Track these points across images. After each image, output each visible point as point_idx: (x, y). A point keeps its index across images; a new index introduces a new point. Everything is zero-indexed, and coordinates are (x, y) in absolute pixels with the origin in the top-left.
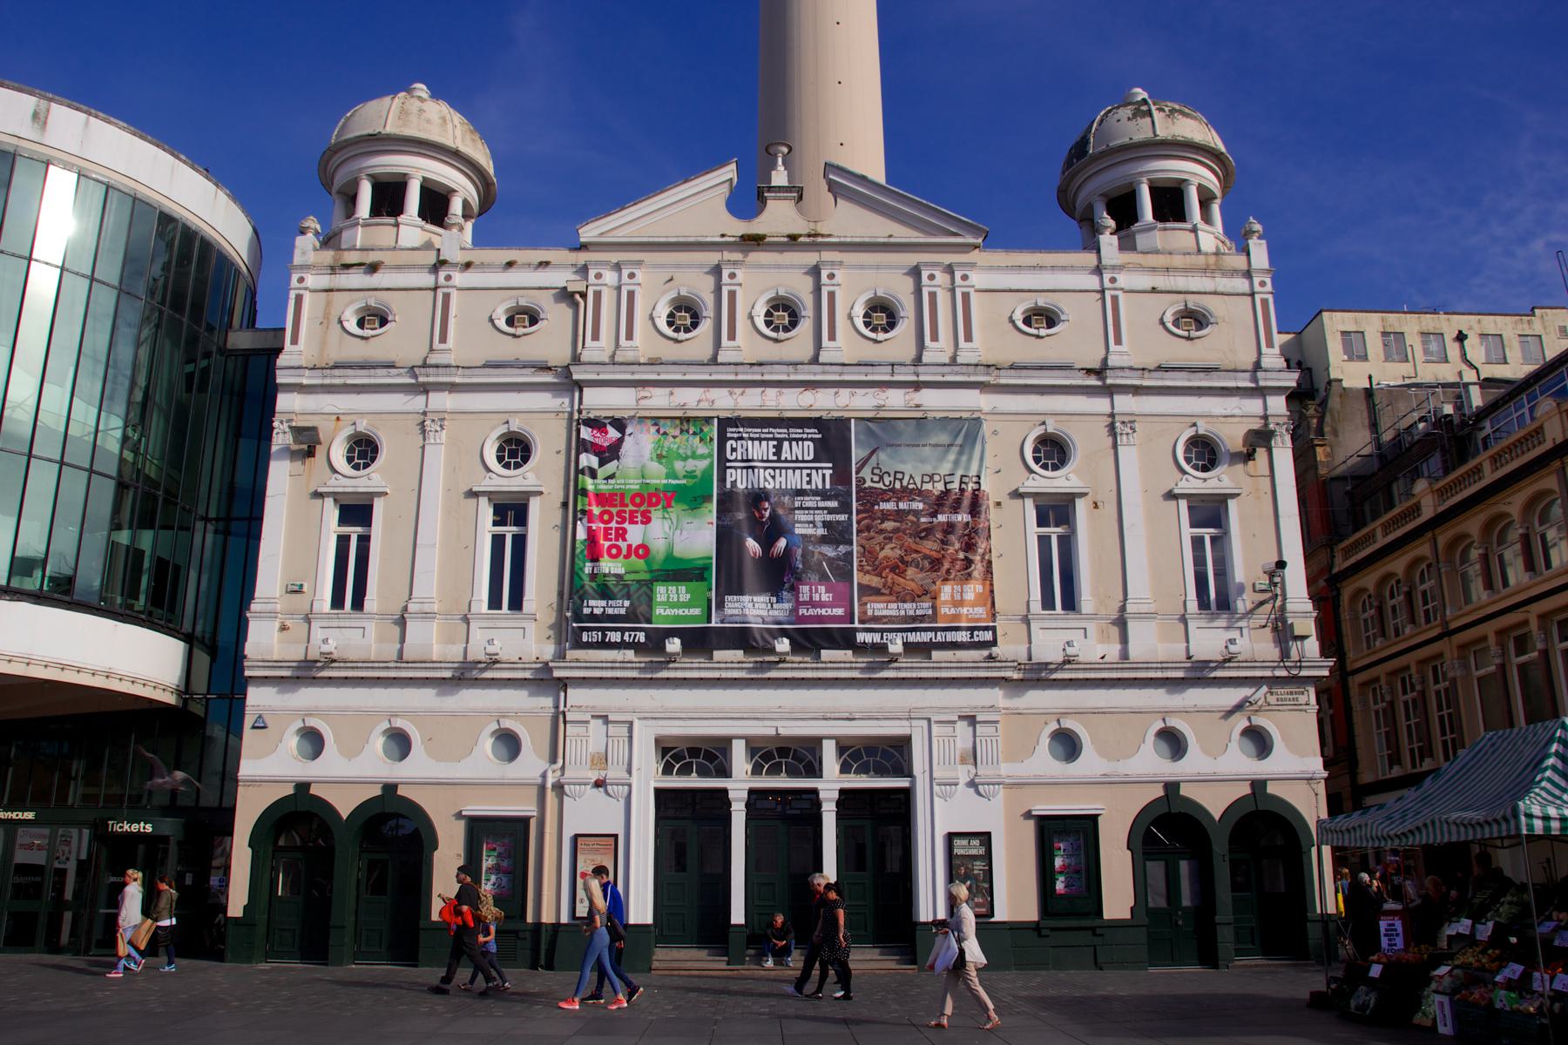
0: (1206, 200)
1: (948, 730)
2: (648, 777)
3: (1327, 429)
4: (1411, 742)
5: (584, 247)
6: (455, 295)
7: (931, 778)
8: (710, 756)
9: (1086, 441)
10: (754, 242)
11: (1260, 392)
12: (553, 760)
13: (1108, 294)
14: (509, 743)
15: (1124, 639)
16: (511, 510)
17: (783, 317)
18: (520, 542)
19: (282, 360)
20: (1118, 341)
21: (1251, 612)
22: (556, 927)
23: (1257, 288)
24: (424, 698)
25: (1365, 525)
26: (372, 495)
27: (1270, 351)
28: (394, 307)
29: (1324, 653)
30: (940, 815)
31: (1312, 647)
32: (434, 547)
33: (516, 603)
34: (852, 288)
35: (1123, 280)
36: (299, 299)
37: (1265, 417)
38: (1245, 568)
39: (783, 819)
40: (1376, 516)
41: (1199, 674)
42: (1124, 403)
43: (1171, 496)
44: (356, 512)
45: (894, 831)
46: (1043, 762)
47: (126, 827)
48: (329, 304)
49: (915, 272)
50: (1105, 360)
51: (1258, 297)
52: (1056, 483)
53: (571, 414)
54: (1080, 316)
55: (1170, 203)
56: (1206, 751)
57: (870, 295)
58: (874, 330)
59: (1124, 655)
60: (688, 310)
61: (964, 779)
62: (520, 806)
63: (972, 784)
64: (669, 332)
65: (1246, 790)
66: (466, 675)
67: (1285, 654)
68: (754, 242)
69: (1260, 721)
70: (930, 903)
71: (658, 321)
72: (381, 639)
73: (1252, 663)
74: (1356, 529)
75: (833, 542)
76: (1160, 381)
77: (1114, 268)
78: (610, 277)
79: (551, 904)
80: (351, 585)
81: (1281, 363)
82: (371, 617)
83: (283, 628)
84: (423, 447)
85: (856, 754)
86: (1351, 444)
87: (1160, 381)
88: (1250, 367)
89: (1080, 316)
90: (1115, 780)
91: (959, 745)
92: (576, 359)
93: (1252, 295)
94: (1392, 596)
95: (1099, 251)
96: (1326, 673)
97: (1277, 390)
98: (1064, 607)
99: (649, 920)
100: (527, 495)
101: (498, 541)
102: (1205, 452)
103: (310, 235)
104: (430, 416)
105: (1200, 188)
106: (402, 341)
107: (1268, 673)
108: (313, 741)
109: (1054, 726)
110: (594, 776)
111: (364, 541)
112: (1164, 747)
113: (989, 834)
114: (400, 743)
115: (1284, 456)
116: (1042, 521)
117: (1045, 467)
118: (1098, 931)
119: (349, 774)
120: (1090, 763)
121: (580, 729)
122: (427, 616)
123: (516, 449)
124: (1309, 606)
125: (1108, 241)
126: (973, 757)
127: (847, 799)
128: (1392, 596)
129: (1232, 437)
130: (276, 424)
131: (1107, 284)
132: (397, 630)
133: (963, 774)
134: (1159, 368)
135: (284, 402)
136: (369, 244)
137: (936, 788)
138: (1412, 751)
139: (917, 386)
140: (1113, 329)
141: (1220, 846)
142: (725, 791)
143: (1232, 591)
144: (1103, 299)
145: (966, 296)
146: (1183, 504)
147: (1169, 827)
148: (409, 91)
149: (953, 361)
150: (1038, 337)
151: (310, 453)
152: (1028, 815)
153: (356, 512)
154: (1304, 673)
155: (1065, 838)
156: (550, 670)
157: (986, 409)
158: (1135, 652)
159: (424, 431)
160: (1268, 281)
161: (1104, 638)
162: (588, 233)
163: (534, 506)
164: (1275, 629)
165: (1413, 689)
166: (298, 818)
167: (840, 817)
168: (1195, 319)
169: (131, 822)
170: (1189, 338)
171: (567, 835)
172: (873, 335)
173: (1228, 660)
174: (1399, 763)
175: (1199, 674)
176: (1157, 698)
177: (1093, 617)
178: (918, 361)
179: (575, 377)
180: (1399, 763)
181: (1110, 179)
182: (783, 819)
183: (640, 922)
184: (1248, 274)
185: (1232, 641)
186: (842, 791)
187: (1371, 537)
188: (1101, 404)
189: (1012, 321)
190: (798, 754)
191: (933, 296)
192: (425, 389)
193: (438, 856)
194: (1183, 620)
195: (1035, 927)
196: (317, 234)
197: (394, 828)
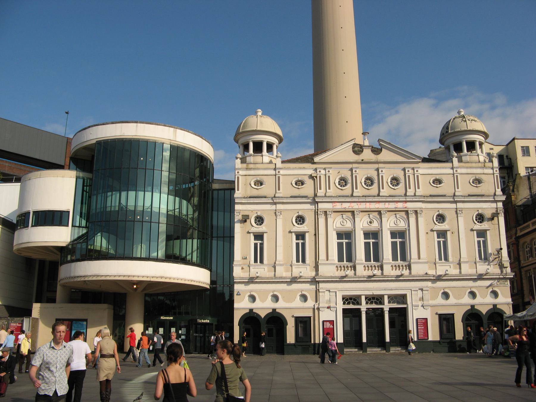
1: (416, 292)
2: (340, 306)
3: (515, 190)
8: (355, 300)
9: (450, 216)
10: (363, 162)
11: (496, 202)
12: (316, 302)
13: (455, 175)
14: (304, 298)
15: (460, 268)
16: (301, 236)
18: (303, 245)
19: (236, 196)
21: (493, 261)
22: (319, 344)
23: (495, 172)
24: (284, 286)
25: (527, 222)
26: (263, 233)
28: (265, 180)
29: (512, 271)
30: (415, 314)
31: (509, 270)
34: (387, 174)
35: (459, 171)
36: (238, 178)
37: (497, 208)
39: (375, 317)
41: (480, 277)
42: (460, 205)
43: (472, 230)
44: (259, 237)
46: (440, 300)
47: (203, 321)
48: (246, 180)
50: (455, 193)
51: (495, 175)
53: (315, 210)
54: (448, 181)
55: (471, 146)
56: (481, 297)
57: (392, 176)
58: (393, 186)
59: (460, 272)
61: (420, 305)
63: (423, 306)
64: (339, 187)
66: (294, 280)
67: (502, 272)
68: (363, 162)
69: (496, 289)
72: (269, 271)
73: (493, 275)
74: (524, 223)
77: (457, 168)
78: (323, 172)
79: (318, 337)
80: (259, 257)
81: (501, 193)
83: (242, 268)
85: (393, 298)
86: (522, 196)
88: (493, 194)
89: (448, 181)
90: (458, 305)
92: (316, 195)
93: (494, 174)
98: (445, 260)
100: (305, 233)
101: (297, 244)
102: (481, 218)
105: (479, 142)
106: (267, 189)
107: (498, 277)
108: (253, 298)
109: (443, 291)
110: (327, 305)
111: (262, 245)
112: (471, 296)
113: (427, 319)
114: (276, 298)
115: (502, 219)
116: (438, 237)
117: (439, 223)
119: (263, 307)
120: (452, 300)
122: (281, 265)
123: (301, 219)
125: (455, 160)
126: (422, 299)
129: (488, 214)
131: (455, 172)
132: (273, 268)
133: (420, 303)
135: (237, 207)
139: (406, 202)
140: (456, 185)
143: (488, 256)
145: (418, 176)
146: (475, 232)
147: (472, 316)
148: (256, 113)
149: (415, 195)
151: (245, 221)
153: (259, 237)
154: (507, 277)
155: (446, 320)
156: (315, 279)
157: (424, 207)
158: (463, 272)
159: (276, 215)
160: (498, 170)
161: (455, 268)
163: (307, 235)
164: (499, 265)
166: (250, 318)
168: (478, 181)
169: (204, 320)
170: (477, 187)
172: (393, 187)
173: (486, 274)
175: (480, 277)
176: (470, 283)
177: (452, 262)
178: (405, 195)
181: (456, 139)
182: (375, 317)
184: (493, 168)
185: (488, 269)
186: (390, 308)
187: (528, 226)
188: (453, 206)
189: (430, 183)
190: (379, 299)
191: (409, 176)
192: (275, 204)
194: (475, 263)
197: (276, 320)
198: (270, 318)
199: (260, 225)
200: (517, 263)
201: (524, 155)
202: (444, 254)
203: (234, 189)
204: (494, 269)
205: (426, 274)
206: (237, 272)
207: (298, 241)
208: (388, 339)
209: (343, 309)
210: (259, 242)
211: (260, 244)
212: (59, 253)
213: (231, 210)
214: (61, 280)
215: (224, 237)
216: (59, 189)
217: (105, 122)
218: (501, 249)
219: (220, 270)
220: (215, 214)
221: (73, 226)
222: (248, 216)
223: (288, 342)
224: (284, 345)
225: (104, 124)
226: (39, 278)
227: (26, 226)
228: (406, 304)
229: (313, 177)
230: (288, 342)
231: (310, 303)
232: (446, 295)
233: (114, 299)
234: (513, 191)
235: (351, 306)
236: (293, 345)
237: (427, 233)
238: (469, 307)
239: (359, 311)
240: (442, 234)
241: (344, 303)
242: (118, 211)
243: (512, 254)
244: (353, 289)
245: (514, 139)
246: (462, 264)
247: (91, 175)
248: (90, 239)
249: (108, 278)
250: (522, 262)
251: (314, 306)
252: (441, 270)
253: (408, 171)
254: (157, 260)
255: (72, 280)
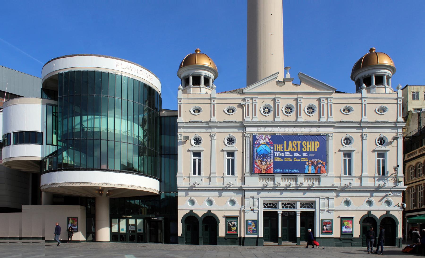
0: (388, 78)
1: (323, 200)
2: (262, 210)
4: (420, 201)
7: (320, 209)
11: (396, 127)
12: (242, 205)
14: (233, 202)
16: (231, 154)
18: (233, 161)
19: (178, 120)
20: (365, 115)
25: (414, 150)
30: (321, 216)
32: (215, 163)
33: (233, 173)
34: (305, 103)
36: (180, 106)
38: (389, 168)
39: (289, 218)
40: (417, 148)
42: (365, 130)
44: (197, 154)
49: (319, 100)
50: (362, 120)
52: (348, 148)
54: (357, 109)
61: (326, 210)
63: (328, 211)
64: (263, 113)
66: (225, 189)
75: (294, 156)
80: (197, 169)
81: (402, 120)
82: (203, 177)
83: (184, 179)
85: (303, 205)
89: (357, 109)
92: (244, 120)
94: (419, 167)
95: (362, 93)
97: (400, 127)
98: (348, 175)
116: (345, 155)
117: (346, 144)
119: (200, 209)
125: (364, 91)
127: (302, 213)
128: (419, 167)
135: (179, 130)
138: (420, 204)
139: (319, 126)
140: (363, 112)
141: (379, 224)
147: (368, 221)
150: (346, 115)
153: (197, 154)
157: (334, 131)
160: (402, 100)
165: (422, 189)
166: (191, 219)
167: (301, 217)
174: (416, 206)
175: (378, 190)
177: (355, 177)
180: (416, 206)
182: (289, 218)
184: (397, 99)
186: (283, 212)
190: (292, 205)
191: (323, 105)
195: (339, 239)
197: (211, 220)
198: (194, 217)
199: (198, 144)
201: (414, 99)
202: (348, 169)
203: (177, 116)
204: (390, 184)
206: (181, 182)
207: (228, 158)
209: (264, 211)
210: (197, 158)
211: (198, 160)
212: (39, 166)
213: (175, 134)
214: (42, 186)
215: (170, 155)
216: (32, 114)
217: (64, 55)
218: (398, 166)
219: (167, 181)
220: (163, 136)
221: (47, 144)
222: (188, 137)
223: (220, 236)
224: (216, 238)
225: (64, 57)
226: (26, 184)
227: (9, 144)
228: (315, 208)
229: (242, 105)
230: (220, 236)
231: (238, 205)
233: (86, 200)
235: (270, 209)
236: (224, 238)
237: (336, 153)
238: (366, 213)
239: (276, 213)
240: (348, 154)
241: (265, 207)
242: (80, 132)
243: (406, 171)
245: (407, 86)
246: (363, 179)
247: (57, 102)
248: (59, 155)
249: (74, 185)
251: (241, 208)
252: (345, 182)
254: (114, 171)
255: (53, 186)
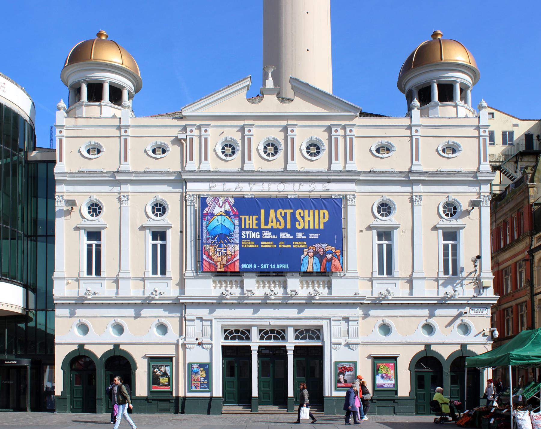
1: (338, 323)
2: (219, 341)
3: (535, 179)
5: (182, 118)
6: (129, 140)
12: (181, 334)
14: (163, 328)
16: (159, 235)
17: (229, 150)
27: (485, 163)
30: (333, 357)
32: (126, 251)
34: (301, 136)
36: (61, 141)
39: (273, 357)
44: (94, 235)
45: (317, 361)
46: (379, 336)
54: (401, 147)
60: (273, 145)
61: (344, 343)
62: (169, 351)
63: (347, 345)
64: (222, 156)
65: (111, 347)
66: (147, 303)
70: (330, 390)
71: (217, 152)
76: (437, 179)
78: (196, 132)
80: (94, 263)
82: (104, 278)
83: (68, 283)
84: (120, 208)
85: (300, 333)
87: (437, 179)
89: (401, 147)
91: (342, 329)
96: (496, 302)
98: (387, 274)
99: (221, 395)
101: (154, 247)
103: (62, 111)
104: (122, 194)
105: (461, 84)
109: (381, 322)
117: (382, 215)
118: (395, 401)
119: (100, 342)
121: (192, 323)
123: (160, 208)
124: (491, 275)
127: (297, 349)
130: (56, 197)
134: (80, 172)
135: (58, 188)
136: (88, 116)
137: (333, 346)
139: (329, 181)
141: (446, 370)
142: (249, 347)
143: (459, 270)
144: (412, 141)
145: (351, 139)
147: (427, 366)
152: (369, 357)
153: (94, 235)
157: (357, 190)
162: (187, 112)
167: (295, 356)
171: (187, 363)
179: (184, 177)
182: (273, 357)
183: (217, 396)
186: (295, 347)
191: (337, 139)
193: (137, 372)
196: (64, 109)
197: (119, 364)
200: (529, 288)
205: (356, 294)
208: (255, 393)
209: (223, 347)
210: (94, 243)
213: (50, 194)
229: (180, 140)
231: (173, 335)
232: (386, 329)
234: (532, 181)
236: (146, 399)
237: (361, 231)
239: (248, 349)
244: (240, 317)
250: (536, 286)
251: (178, 341)
253: (336, 131)
